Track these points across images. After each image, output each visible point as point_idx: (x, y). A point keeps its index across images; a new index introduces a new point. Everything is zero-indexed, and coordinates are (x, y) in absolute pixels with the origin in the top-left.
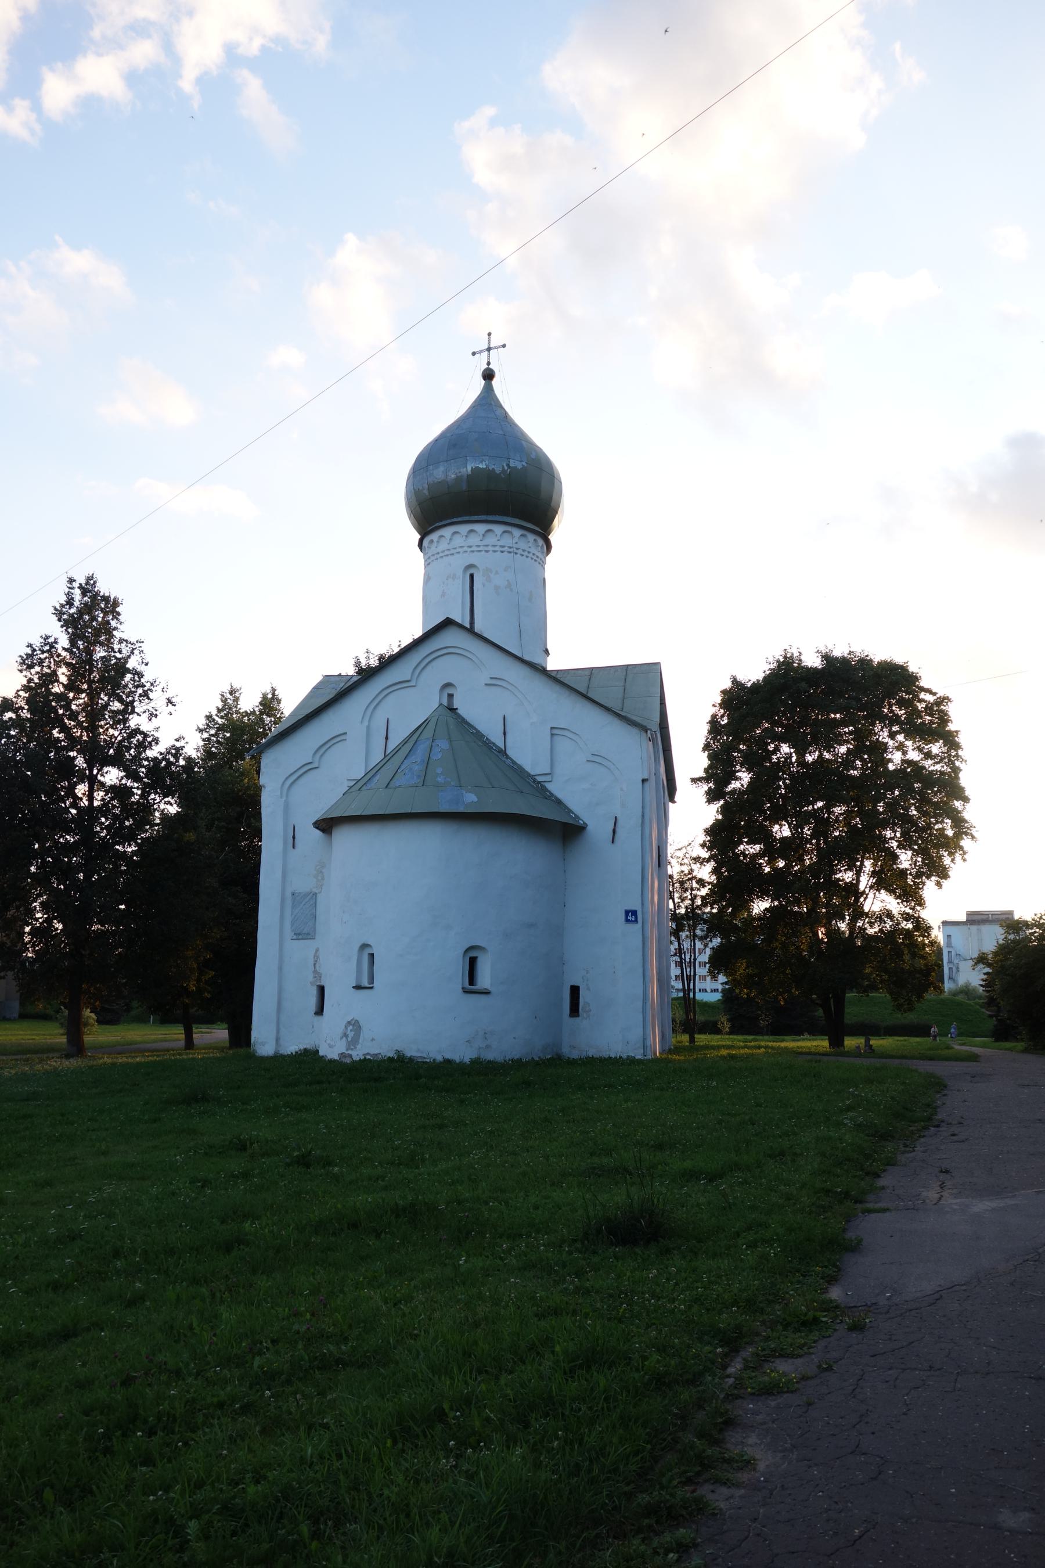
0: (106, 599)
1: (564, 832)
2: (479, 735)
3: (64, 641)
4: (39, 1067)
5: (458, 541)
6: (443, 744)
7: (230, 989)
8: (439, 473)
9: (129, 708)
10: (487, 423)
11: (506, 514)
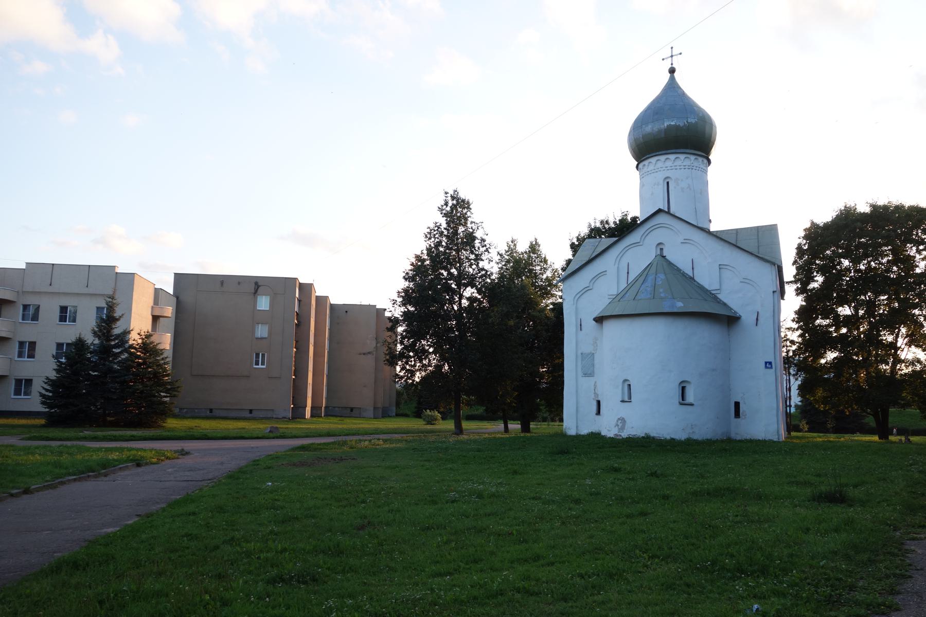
0: (463, 201)
1: (728, 320)
2: (679, 270)
3: (444, 225)
4: (79, 457)
5: (660, 164)
6: (662, 276)
7: (552, 399)
8: (649, 129)
9: (478, 258)
10: (673, 97)
11: (686, 148)
